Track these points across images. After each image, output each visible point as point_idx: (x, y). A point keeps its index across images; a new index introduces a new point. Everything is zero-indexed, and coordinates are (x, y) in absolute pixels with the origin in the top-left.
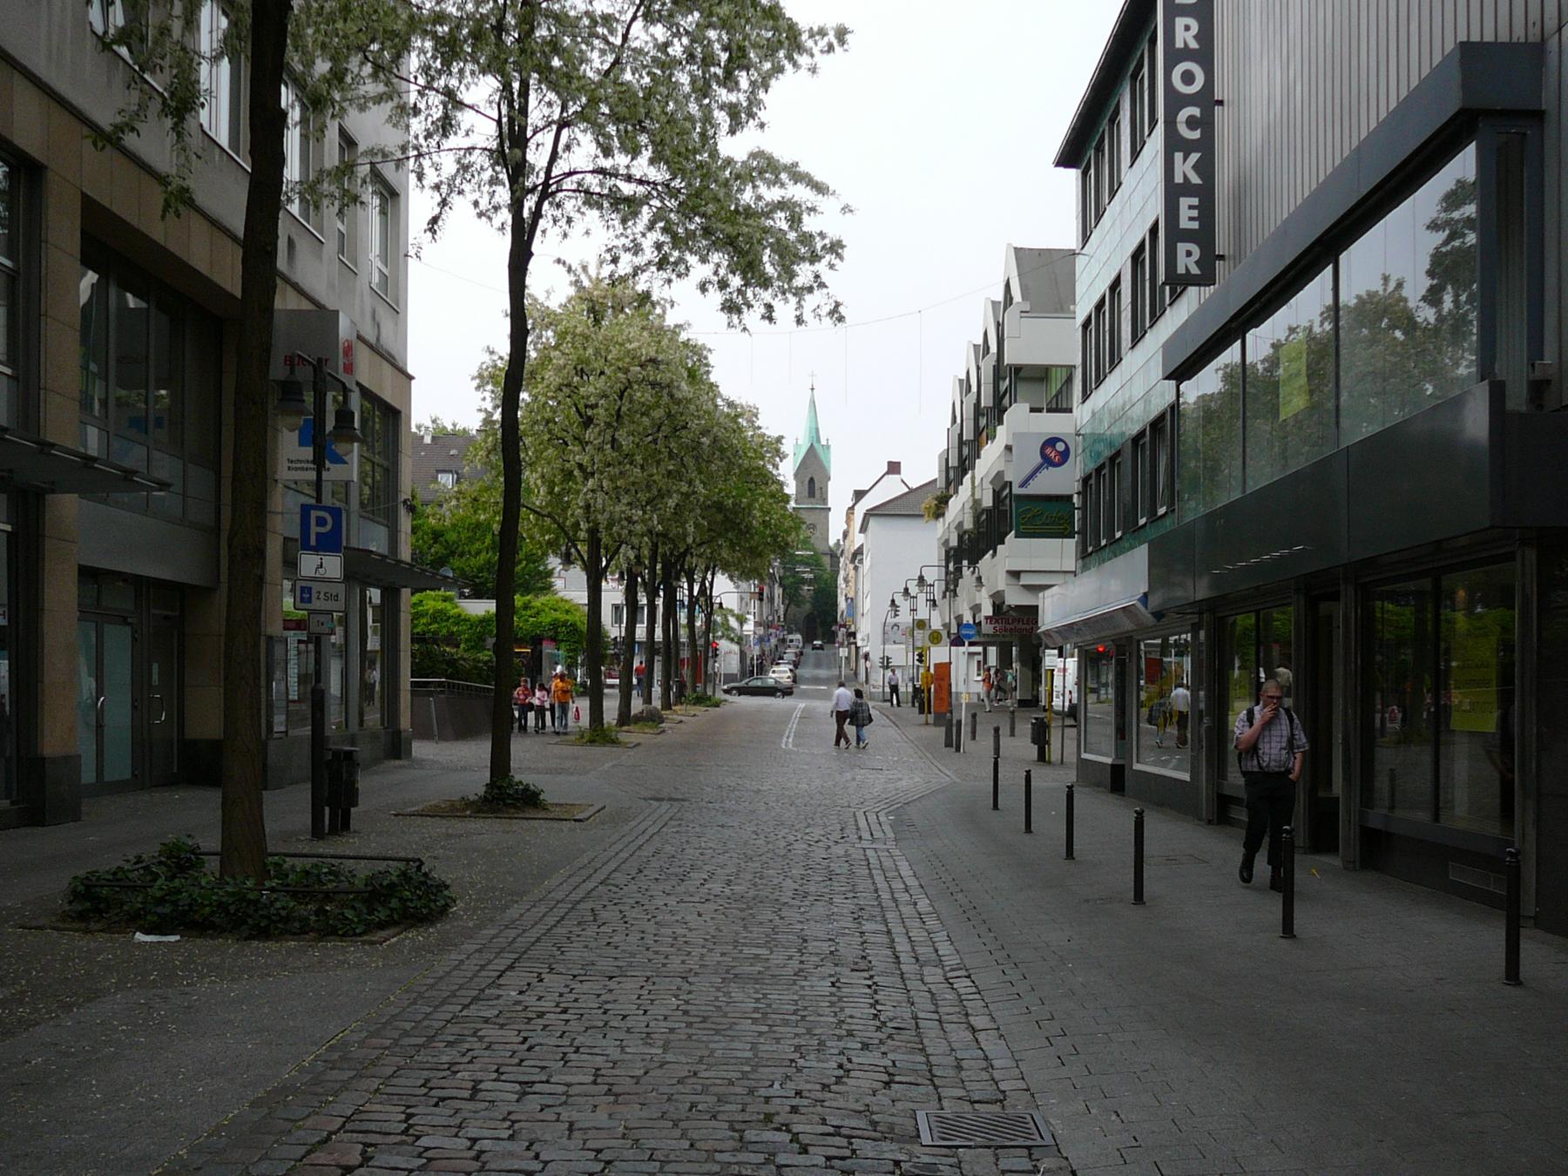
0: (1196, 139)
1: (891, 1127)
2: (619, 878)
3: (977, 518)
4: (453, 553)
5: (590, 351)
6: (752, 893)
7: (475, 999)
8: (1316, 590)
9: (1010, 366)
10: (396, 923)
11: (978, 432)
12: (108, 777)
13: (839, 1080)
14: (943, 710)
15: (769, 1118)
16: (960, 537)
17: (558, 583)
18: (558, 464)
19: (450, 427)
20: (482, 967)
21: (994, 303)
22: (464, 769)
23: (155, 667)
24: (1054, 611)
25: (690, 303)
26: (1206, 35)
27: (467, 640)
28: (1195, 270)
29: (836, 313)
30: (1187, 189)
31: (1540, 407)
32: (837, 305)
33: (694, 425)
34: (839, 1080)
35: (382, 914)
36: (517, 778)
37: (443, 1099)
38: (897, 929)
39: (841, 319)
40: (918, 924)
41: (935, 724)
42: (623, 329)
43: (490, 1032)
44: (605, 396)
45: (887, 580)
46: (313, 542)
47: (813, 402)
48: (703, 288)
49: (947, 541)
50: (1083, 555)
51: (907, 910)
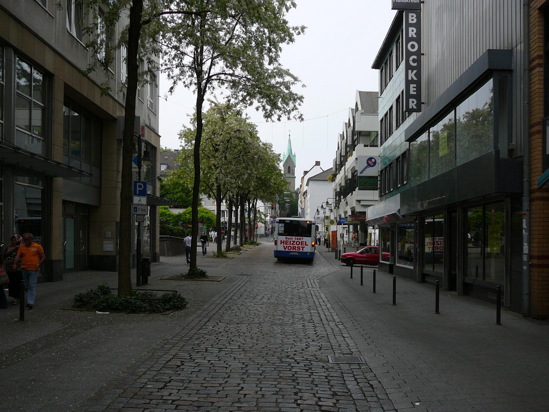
0: (415, 66)
1: (321, 359)
2: (235, 298)
3: (346, 182)
4: (167, 193)
5: (217, 127)
6: (276, 302)
7: (200, 329)
8: (449, 209)
9: (357, 131)
10: (172, 309)
11: (346, 153)
12: (67, 267)
13: (306, 348)
14: (335, 246)
15: (288, 356)
16: (340, 188)
17: (203, 203)
18: (207, 164)
19: (164, 149)
20: (200, 321)
21: (352, 109)
22: (177, 265)
23: (81, 231)
24: (371, 214)
25: (253, 113)
26: (418, 33)
27: (172, 223)
28: (415, 107)
29: (301, 118)
30: (413, 82)
31: (511, 157)
32: (302, 115)
33: (252, 151)
34: (306, 348)
35: (168, 307)
36: (198, 268)
37: (198, 352)
38: (321, 312)
39: (302, 119)
40: (327, 311)
41: (332, 252)
42: (232, 122)
43: (207, 337)
44: (222, 142)
45: (315, 202)
46: (138, 193)
47: (290, 141)
48: (257, 109)
49: (336, 189)
50: (381, 196)
51: (324, 307)
